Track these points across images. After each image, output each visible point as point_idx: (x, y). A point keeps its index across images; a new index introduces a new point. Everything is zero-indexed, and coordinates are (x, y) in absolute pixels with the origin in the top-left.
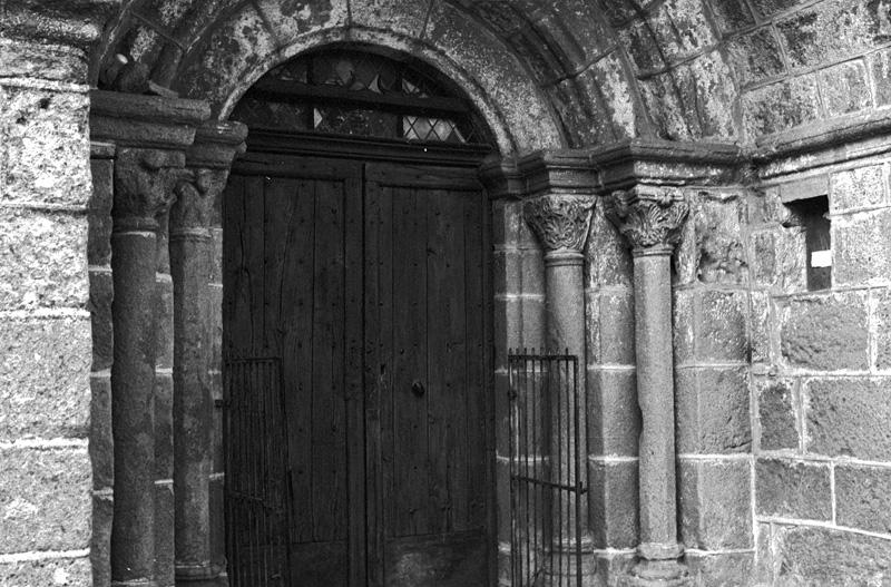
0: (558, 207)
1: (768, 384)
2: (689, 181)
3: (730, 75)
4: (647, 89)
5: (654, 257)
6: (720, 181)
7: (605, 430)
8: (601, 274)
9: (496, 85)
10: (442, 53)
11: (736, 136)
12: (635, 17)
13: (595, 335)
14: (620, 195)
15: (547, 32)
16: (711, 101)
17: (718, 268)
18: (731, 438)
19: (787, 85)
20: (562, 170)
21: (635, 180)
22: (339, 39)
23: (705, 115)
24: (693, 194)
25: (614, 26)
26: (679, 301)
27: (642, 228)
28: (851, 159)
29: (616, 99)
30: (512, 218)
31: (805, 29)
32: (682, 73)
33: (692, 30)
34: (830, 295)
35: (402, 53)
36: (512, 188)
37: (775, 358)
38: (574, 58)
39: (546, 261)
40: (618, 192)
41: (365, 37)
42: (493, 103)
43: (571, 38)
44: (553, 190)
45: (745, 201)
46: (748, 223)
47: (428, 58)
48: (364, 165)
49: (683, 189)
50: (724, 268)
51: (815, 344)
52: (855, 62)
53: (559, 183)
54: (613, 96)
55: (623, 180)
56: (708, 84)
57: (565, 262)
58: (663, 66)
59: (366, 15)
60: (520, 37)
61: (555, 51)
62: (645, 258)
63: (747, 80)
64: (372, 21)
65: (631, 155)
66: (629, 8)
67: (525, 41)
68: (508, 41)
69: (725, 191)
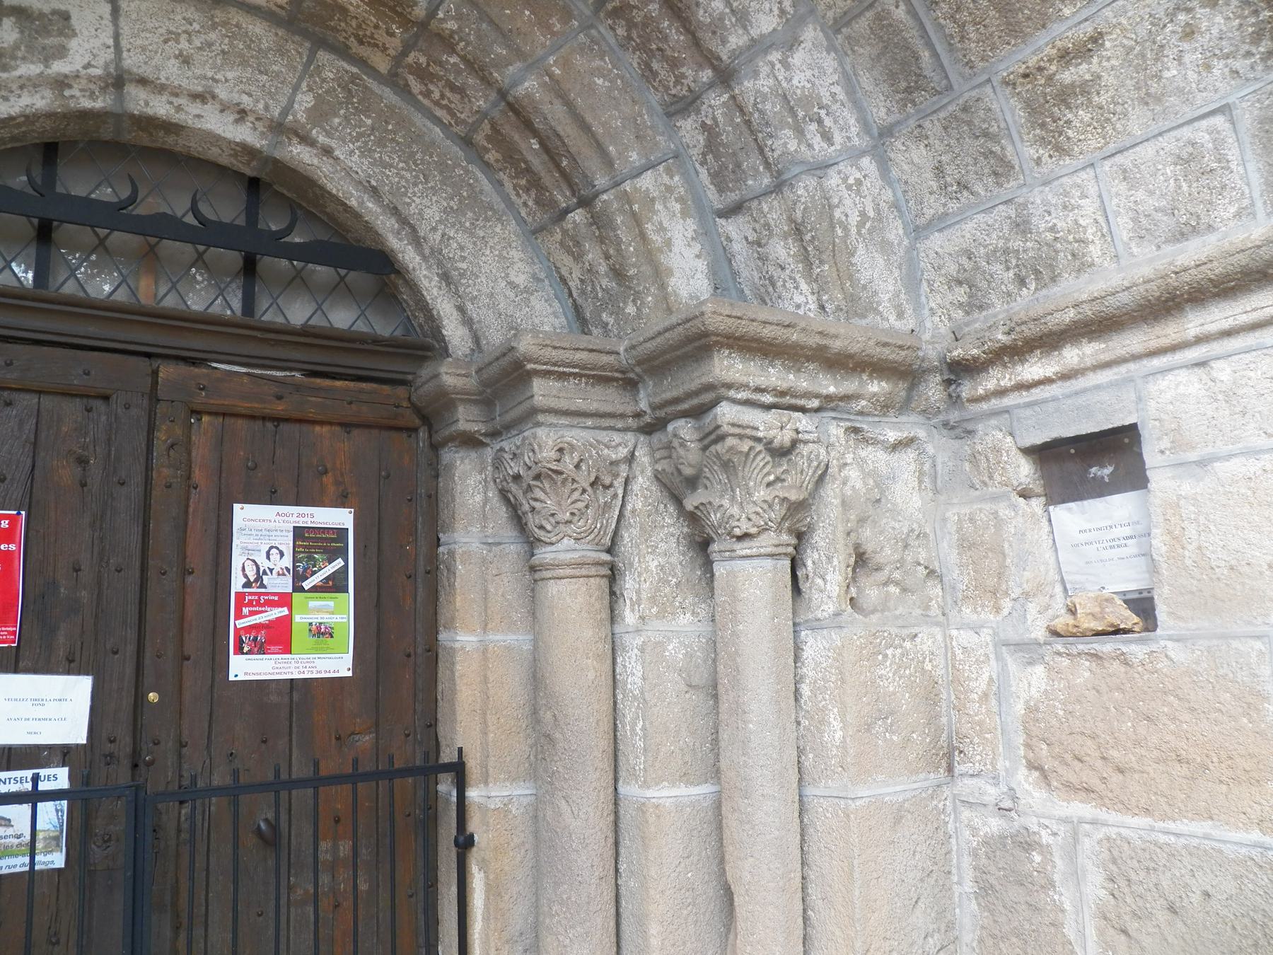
0: (553, 454)
1: (994, 825)
2: (829, 403)
3: (895, 205)
4: (734, 235)
5: (756, 562)
6: (885, 407)
7: (654, 929)
8: (644, 596)
9: (440, 221)
10: (327, 151)
11: (909, 323)
12: (711, 85)
13: (634, 725)
14: (684, 429)
15: (536, 110)
16: (861, 250)
17: (886, 584)
18: (920, 942)
19: (1024, 206)
20: (562, 376)
21: (712, 395)
22: (99, 104)
23: (850, 277)
24: (836, 431)
25: (669, 115)
26: (808, 653)
27: (733, 499)
28: (1200, 340)
29: (675, 249)
30: (471, 482)
31: (1067, 76)
32: (804, 189)
33: (823, 112)
34: (1154, 647)
35: (248, 151)
36: (467, 419)
37: (1010, 772)
38: (591, 164)
39: (533, 569)
40: (681, 422)
41: (160, 107)
42: (435, 257)
43: (585, 127)
44: (541, 418)
45: (930, 449)
46: (936, 491)
47: (301, 162)
48: (155, 373)
49: (816, 418)
50: (897, 584)
51: (1114, 753)
52: (1204, 123)
53: (553, 403)
54: (669, 243)
55: (690, 395)
56: (854, 219)
57: (568, 572)
58: (766, 181)
59: (157, 60)
60: (486, 126)
61: (552, 149)
62: (739, 563)
63: (929, 213)
64: (171, 72)
65: (705, 334)
66: (701, 67)
67: (497, 137)
68: (467, 142)
69: (895, 426)
